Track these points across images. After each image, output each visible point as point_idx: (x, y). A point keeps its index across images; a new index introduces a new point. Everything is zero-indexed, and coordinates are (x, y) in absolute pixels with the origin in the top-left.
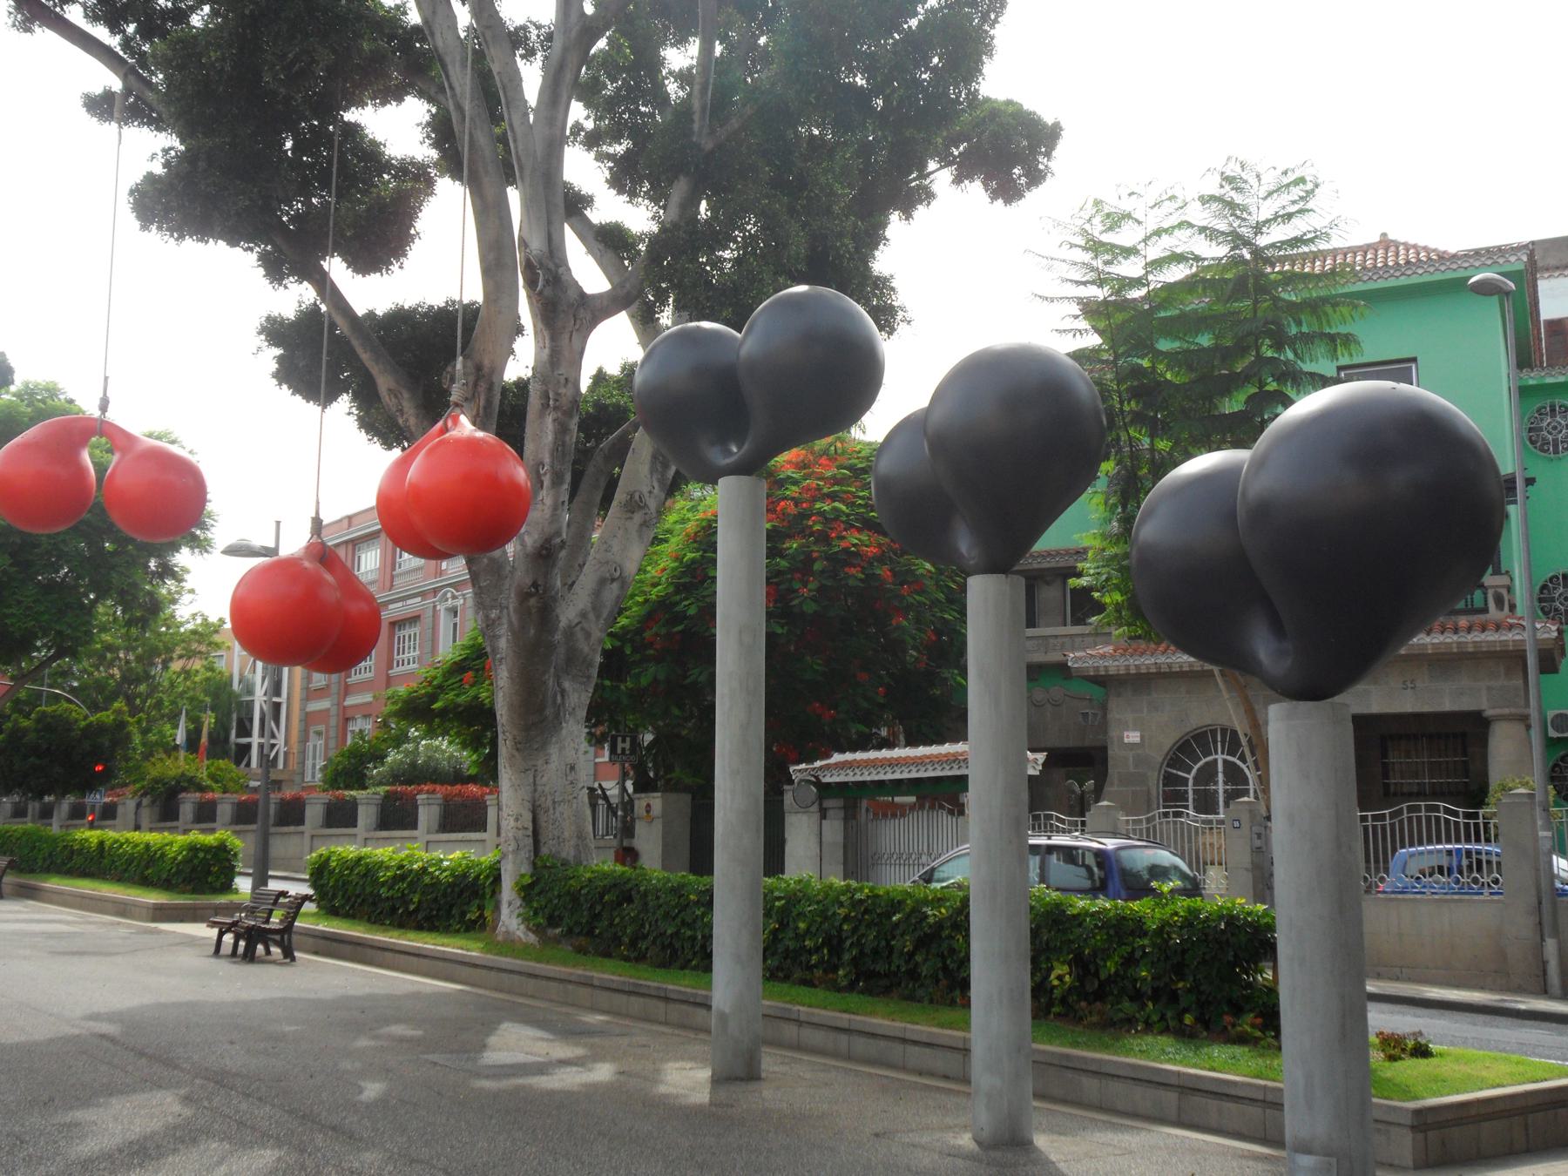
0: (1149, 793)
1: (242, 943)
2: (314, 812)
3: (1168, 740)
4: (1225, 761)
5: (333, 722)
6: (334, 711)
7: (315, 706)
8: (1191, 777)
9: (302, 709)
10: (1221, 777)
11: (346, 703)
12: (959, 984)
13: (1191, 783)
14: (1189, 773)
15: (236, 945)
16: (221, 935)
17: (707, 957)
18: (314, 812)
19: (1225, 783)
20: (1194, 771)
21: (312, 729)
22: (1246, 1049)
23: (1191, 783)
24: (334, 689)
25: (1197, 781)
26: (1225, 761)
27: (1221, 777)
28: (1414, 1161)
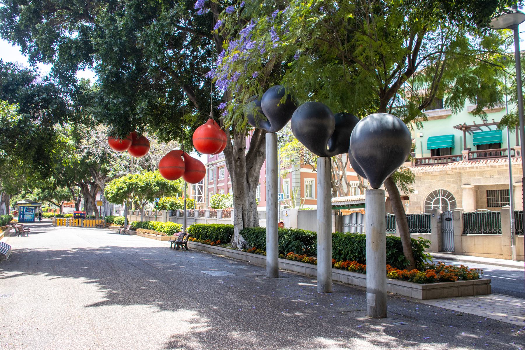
0: (421, 207)
1: (176, 245)
2: (207, 214)
3: (427, 194)
4: (442, 199)
5: (215, 190)
6: (215, 188)
7: (210, 187)
8: (432, 203)
9: (207, 187)
10: (441, 203)
11: (218, 186)
12: (362, 260)
13: (432, 204)
14: (432, 201)
15: (175, 246)
16: (172, 244)
17: (265, 249)
18: (207, 214)
19: (442, 204)
20: (435, 199)
21: (210, 192)
22: (260, 221)
23: (432, 204)
24: (215, 182)
25: (434, 204)
26: (442, 199)
27: (441, 203)
28: (423, 297)
